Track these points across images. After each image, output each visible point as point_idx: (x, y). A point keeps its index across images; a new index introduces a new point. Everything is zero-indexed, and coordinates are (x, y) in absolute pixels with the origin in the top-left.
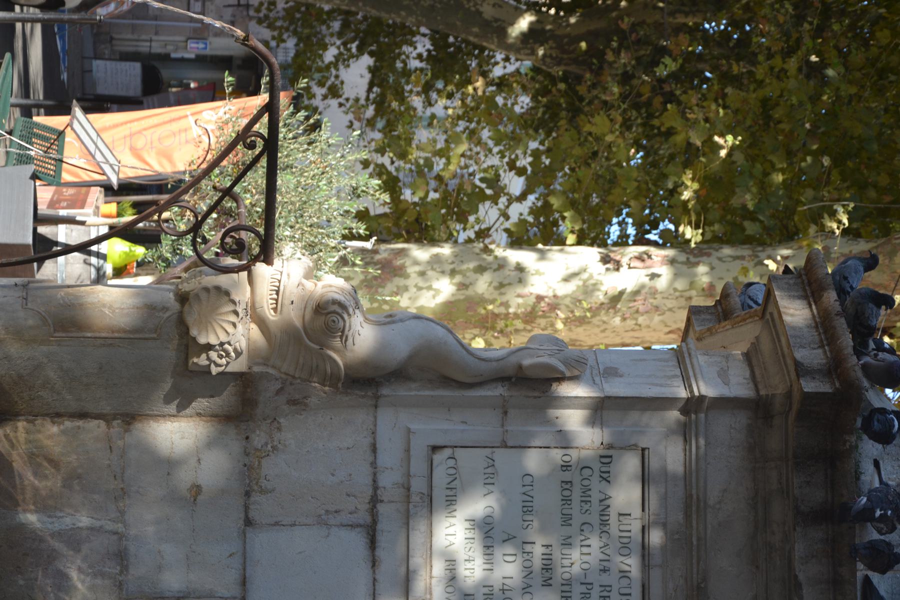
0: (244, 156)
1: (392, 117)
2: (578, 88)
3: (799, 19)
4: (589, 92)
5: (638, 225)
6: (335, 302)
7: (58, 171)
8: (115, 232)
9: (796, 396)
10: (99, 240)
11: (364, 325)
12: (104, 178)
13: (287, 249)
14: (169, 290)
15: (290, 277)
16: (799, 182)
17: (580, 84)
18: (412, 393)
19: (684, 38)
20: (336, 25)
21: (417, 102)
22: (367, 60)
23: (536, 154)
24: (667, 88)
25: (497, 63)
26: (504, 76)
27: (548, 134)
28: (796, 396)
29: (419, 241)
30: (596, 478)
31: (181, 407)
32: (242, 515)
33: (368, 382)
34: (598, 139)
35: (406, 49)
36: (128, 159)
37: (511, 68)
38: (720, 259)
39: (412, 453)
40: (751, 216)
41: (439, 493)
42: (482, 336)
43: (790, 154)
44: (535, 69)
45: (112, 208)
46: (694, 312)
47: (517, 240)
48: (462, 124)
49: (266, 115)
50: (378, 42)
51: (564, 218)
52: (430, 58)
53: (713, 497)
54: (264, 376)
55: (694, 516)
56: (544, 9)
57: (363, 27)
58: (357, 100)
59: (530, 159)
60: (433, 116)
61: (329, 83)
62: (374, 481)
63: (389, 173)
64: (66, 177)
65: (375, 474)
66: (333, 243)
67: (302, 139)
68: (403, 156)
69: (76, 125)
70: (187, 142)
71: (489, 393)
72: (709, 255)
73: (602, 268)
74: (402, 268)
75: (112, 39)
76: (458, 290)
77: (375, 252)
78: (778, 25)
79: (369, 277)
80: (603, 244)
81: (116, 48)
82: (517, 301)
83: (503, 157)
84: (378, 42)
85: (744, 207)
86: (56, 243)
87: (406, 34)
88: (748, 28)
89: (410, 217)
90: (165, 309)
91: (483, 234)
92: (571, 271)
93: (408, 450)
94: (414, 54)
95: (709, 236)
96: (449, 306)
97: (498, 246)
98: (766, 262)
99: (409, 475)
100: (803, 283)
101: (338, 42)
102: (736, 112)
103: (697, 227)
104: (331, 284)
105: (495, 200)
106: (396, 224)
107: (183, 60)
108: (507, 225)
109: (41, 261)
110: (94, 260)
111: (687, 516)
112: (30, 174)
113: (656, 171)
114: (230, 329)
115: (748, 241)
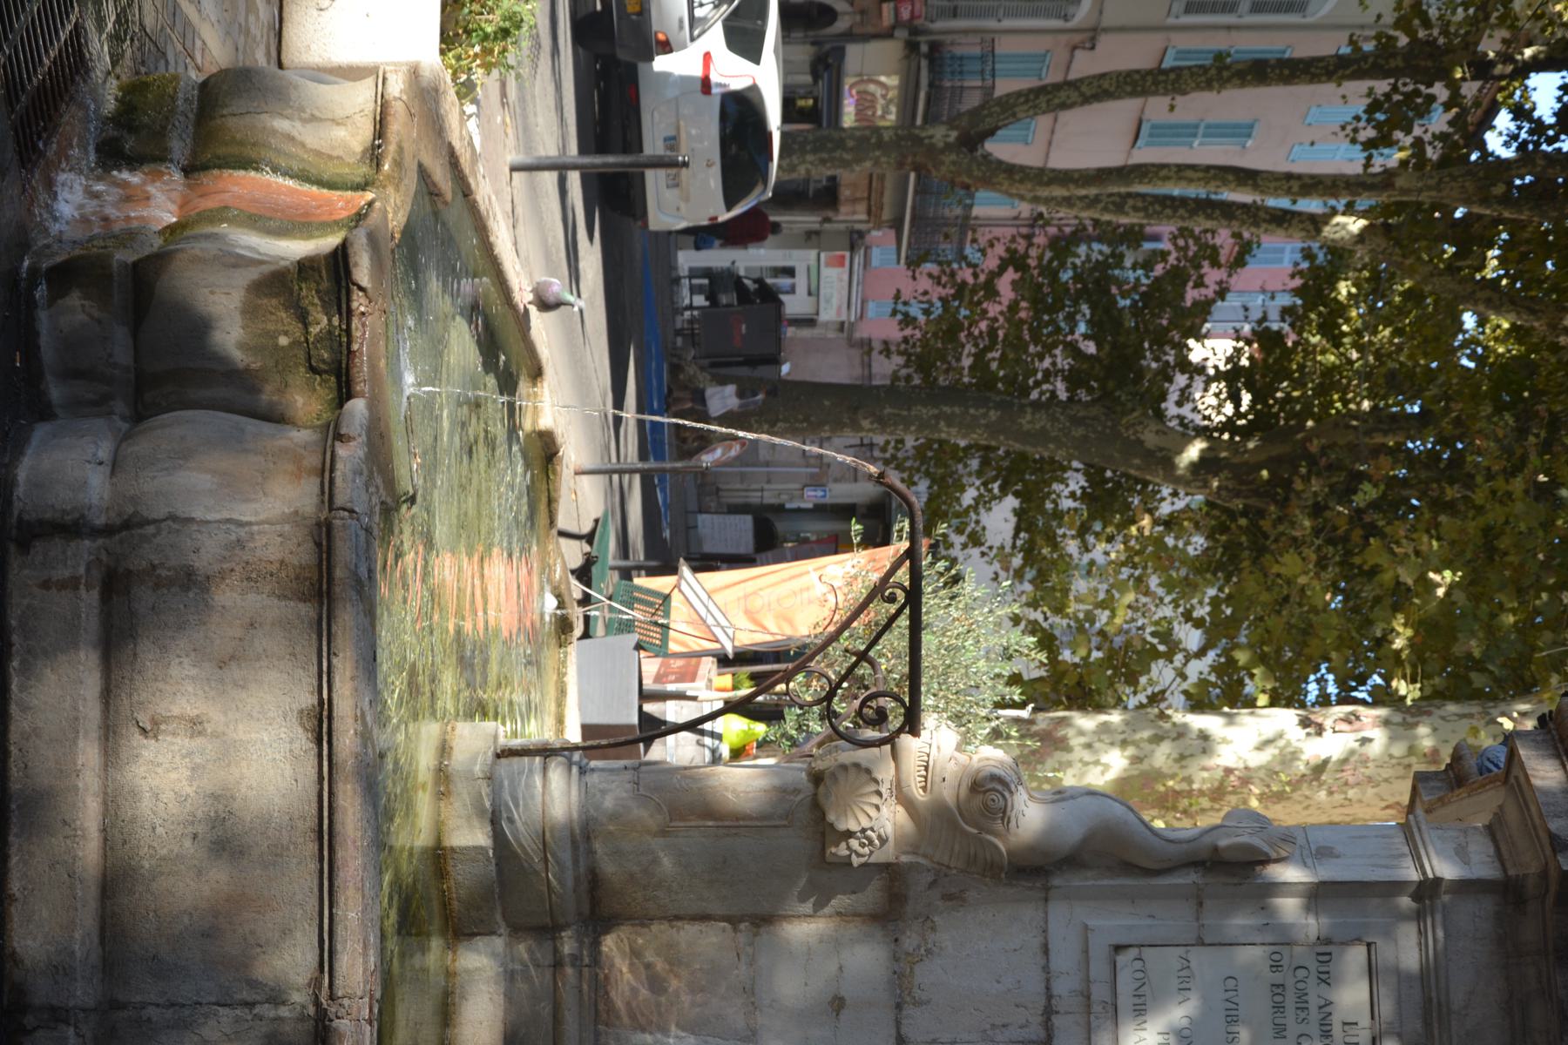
0: (876, 614)
1: (1044, 566)
2: (1262, 523)
3: (1522, 432)
4: (1274, 526)
5: (1341, 683)
6: (994, 778)
7: (665, 639)
8: (731, 707)
9: (1553, 873)
10: (713, 716)
11: (1029, 803)
12: (717, 646)
13: (929, 720)
14: (800, 770)
15: (941, 749)
16: (1533, 625)
17: (1263, 518)
18: (1090, 883)
19: (1385, 461)
20: (974, 464)
21: (1072, 547)
22: (1011, 502)
23: (1215, 602)
24: (1367, 519)
25: (1163, 499)
26: (1172, 514)
27: (1228, 580)
28: (1553, 873)
29: (1082, 708)
30: (1313, 980)
31: (819, 906)
32: (893, 1032)
33: (1037, 871)
34: (1289, 582)
35: (1056, 487)
36: (742, 622)
37: (1180, 504)
38: (1443, 718)
39: (1091, 953)
40: (1479, 666)
41: (1125, 1000)
42: (1161, 817)
43: (1520, 592)
44: (1209, 503)
45: (727, 680)
46: (1420, 779)
47: (1198, 703)
48: (1125, 572)
49: (908, 563)
50: (1023, 480)
51: (1252, 676)
52: (1085, 497)
53: (1458, 998)
54: (912, 866)
55: (1436, 1025)
56: (1216, 435)
57: (1006, 464)
58: (1002, 547)
59: (1208, 609)
60: (1092, 563)
61: (969, 529)
62: (1048, 988)
63: (1043, 630)
64: (673, 647)
65: (1048, 980)
66: (983, 712)
67: (942, 593)
68: (1059, 610)
69: (684, 586)
70: (810, 602)
71: (1181, 881)
72: (1429, 714)
73: (1302, 732)
74: (1064, 739)
75: (718, 490)
76: (1132, 763)
77: (1031, 722)
78: (1497, 440)
79: (1026, 751)
80: (1303, 705)
81: (724, 500)
82: (1202, 776)
83: (1177, 606)
84: (1023, 480)
85: (1469, 656)
86: (665, 722)
87: (1056, 470)
88: (1460, 446)
89: (1070, 680)
90: (797, 791)
91: (1155, 699)
92: (1264, 737)
93: (1086, 951)
94: (1066, 493)
95: (1428, 691)
96: (1123, 782)
97: (1176, 710)
98: (1500, 720)
99: (1088, 981)
100: (1553, 739)
101: (978, 483)
102: (1453, 543)
103: (1414, 681)
104: (991, 756)
105: (1169, 657)
106: (1055, 690)
107: (799, 510)
108: (1185, 686)
109: (648, 741)
110: (708, 741)
111: (1427, 1024)
112: (633, 644)
113: (1360, 615)
114: (872, 812)
115: (1476, 695)
